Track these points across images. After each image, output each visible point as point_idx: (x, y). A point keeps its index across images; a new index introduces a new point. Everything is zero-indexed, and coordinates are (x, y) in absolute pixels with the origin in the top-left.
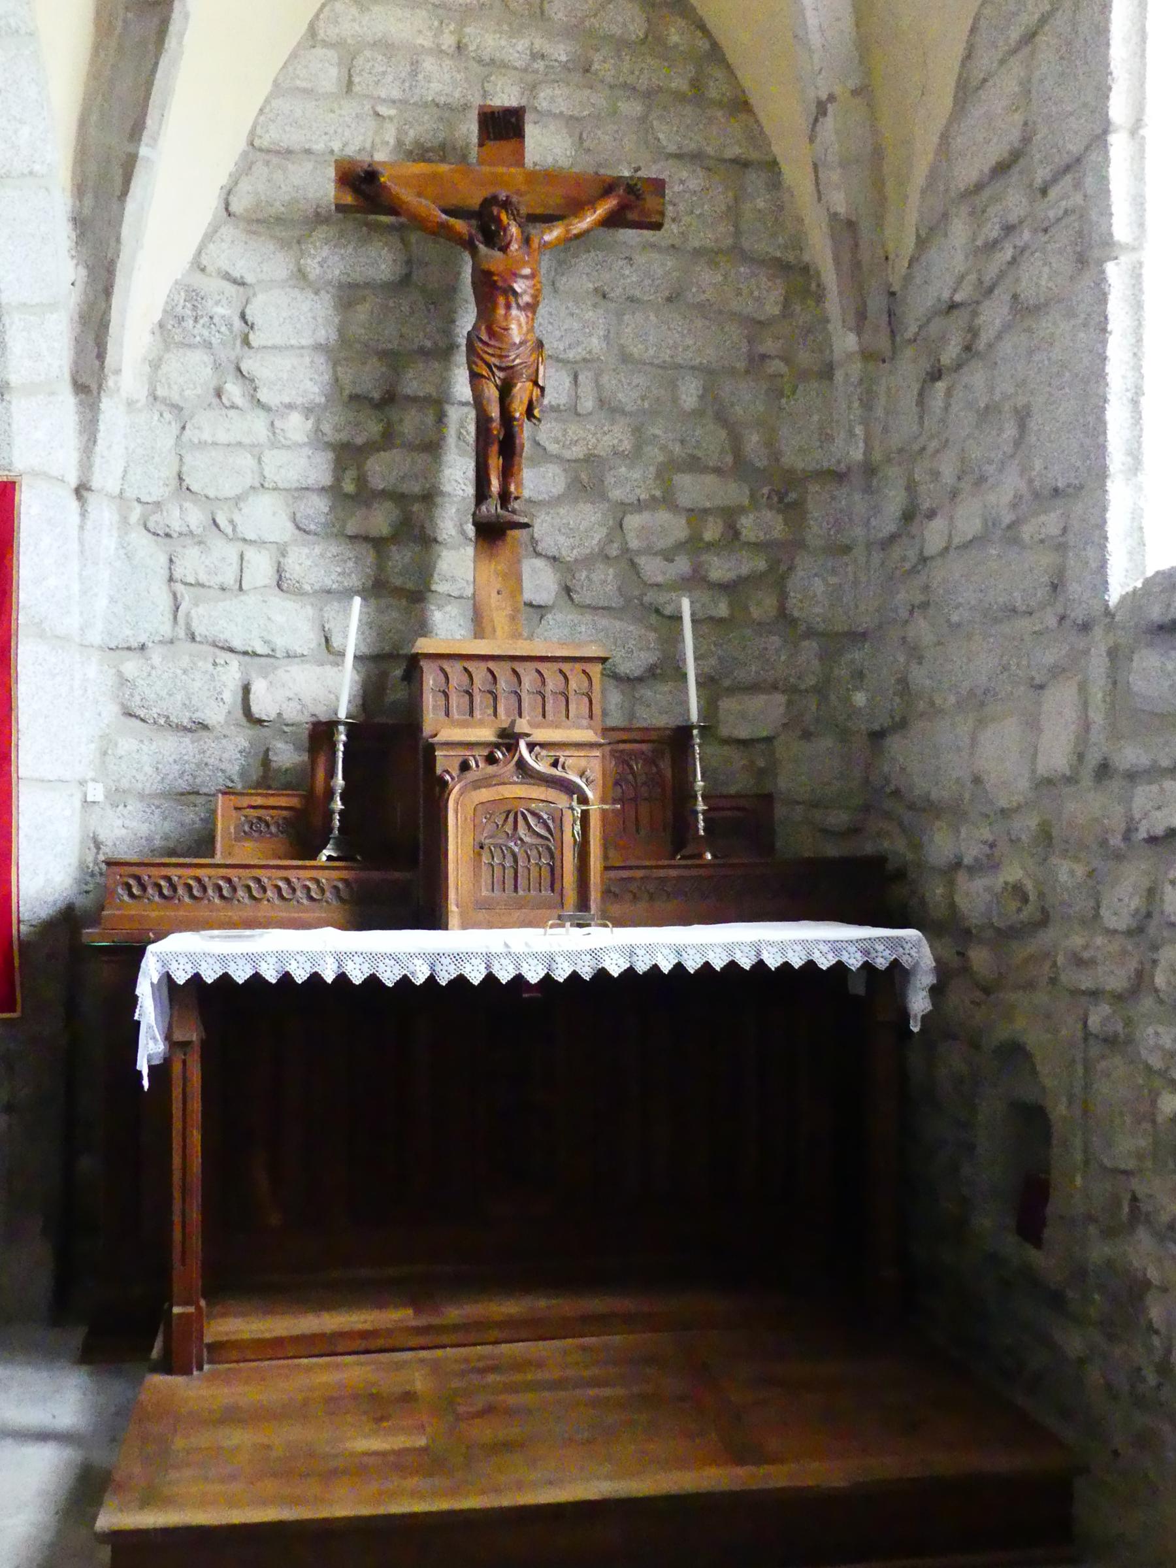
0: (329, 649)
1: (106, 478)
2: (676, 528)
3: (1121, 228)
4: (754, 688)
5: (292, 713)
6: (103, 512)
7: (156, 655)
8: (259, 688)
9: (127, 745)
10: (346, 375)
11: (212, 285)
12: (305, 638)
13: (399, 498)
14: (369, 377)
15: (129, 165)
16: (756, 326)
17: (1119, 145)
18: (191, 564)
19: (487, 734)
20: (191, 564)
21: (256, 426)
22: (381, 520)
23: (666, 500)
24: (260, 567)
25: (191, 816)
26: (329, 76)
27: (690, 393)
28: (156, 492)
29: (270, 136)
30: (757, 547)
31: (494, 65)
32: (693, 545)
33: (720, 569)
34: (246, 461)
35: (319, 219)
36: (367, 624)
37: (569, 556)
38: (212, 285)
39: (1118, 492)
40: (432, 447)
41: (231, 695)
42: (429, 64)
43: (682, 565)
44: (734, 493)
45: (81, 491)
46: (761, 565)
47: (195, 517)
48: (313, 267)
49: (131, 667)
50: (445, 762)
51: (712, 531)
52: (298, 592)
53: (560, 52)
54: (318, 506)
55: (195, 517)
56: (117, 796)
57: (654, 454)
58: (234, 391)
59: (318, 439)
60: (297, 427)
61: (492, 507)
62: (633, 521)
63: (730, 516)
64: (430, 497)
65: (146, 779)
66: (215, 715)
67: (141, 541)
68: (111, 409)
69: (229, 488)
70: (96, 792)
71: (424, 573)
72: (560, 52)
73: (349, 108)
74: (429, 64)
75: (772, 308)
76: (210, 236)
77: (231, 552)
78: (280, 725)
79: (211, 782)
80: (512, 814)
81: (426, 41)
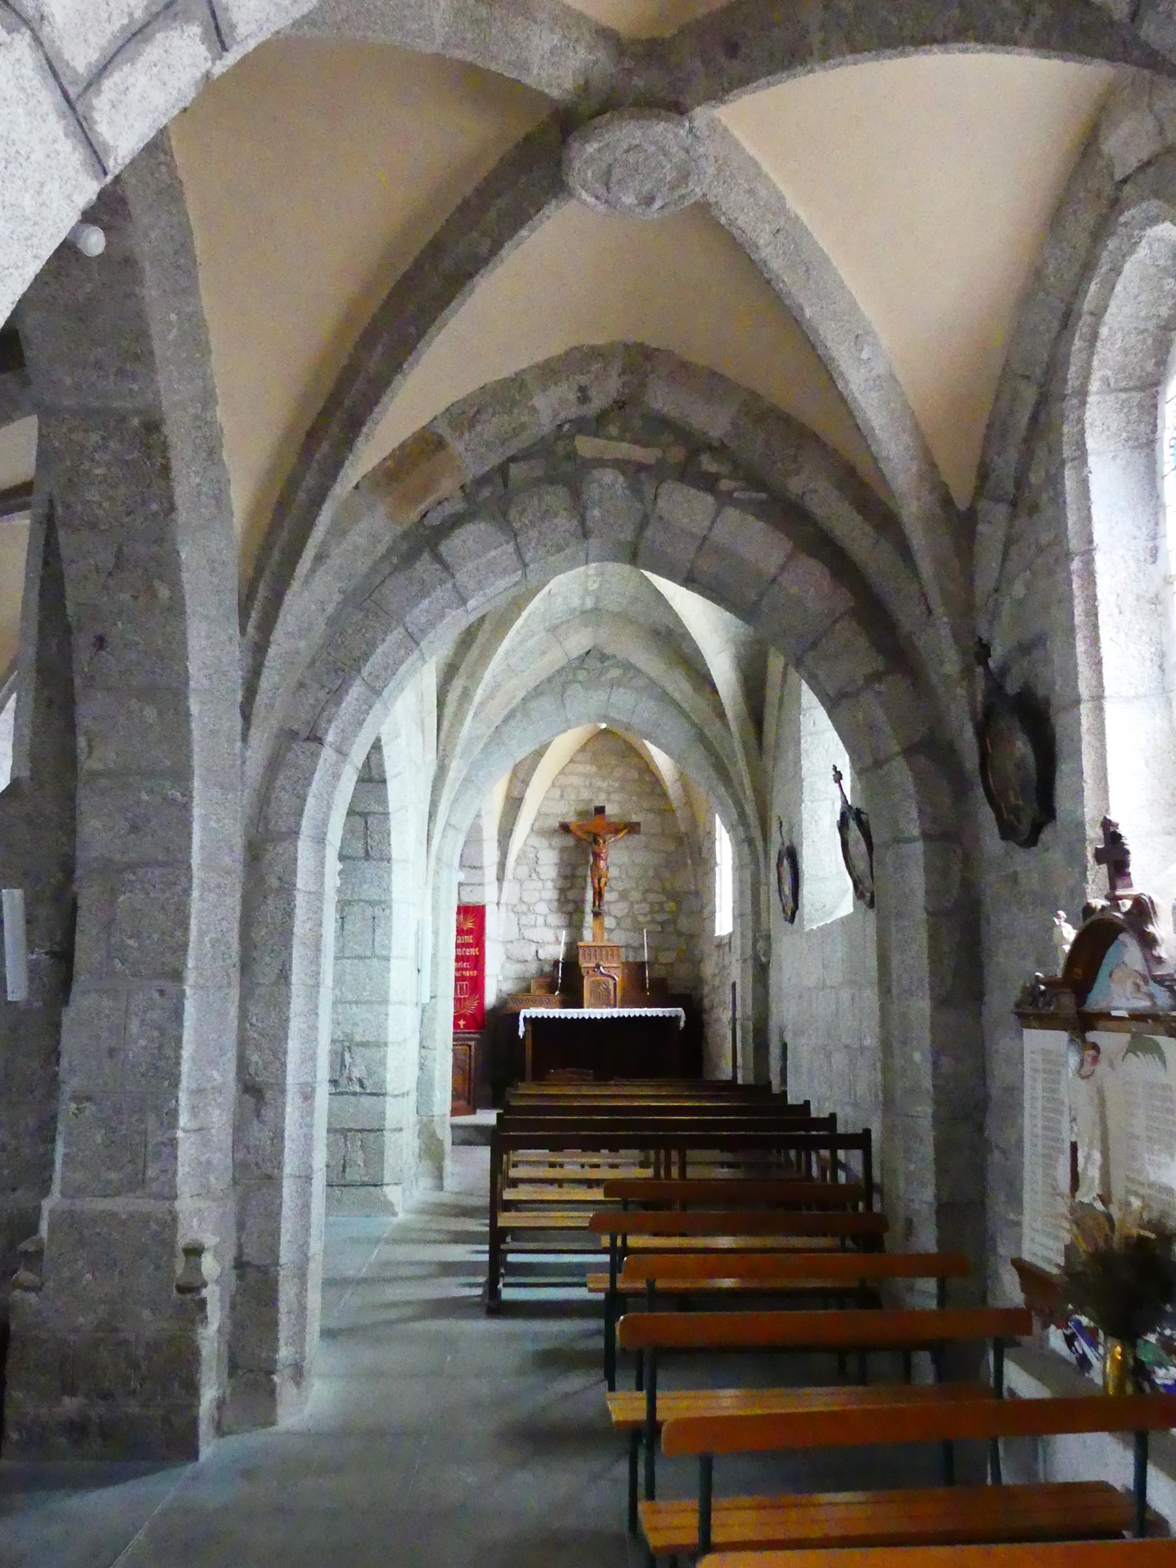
0: (558, 942)
1: (503, 901)
2: (647, 908)
3: (718, 861)
4: (668, 949)
5: (549, 958)
6: (503, 908)
7: (515, 943)
8: (540, 951)
9: (508, 966)
10: (565, 857)
11: (528, 849)
12: (552, 938)
13: (575, 902)
14: (568, 872)
15: (511, 830)
16: (669, 854)
17: (717, 843)
18: (524, 920)
19: (593, 965)
20: (524, 920)
21: (539, 885)
22: (570, 907)
23: (644, 900)
24: (541, 920)
25: (524, 984)
26: (557, 793)
27: (651, 873)
28: (515, 902)
29: (543, 810)
30: (670, 912)
31: (599, 789)
32: (651, 912)
33: (659, 918)
34: (537, 894)
35: (555, 831)
36: (568, 935)
37: (619, 916)
38: (528, 849)
39: (717, 915)
40: (584, 888)
41: (533, 953)
42: (582, 790)
43: (649, 918)
44: (663, 898)
45: (498, 904)
46: (670, 917)
47: (525, 908)
48: (554, 843)
49: (509, 946)
50: (584, 972)
51: (657, 908)
52: (550, 926)
53: (617, 785)
54: (556, 904)
55: (525, 908)
56: (506, 979)
57: (641, 888)
58: (534, 875)
59: (555, 887)
60: (550, 885)
61: (596, 909)
62: (636, 906)
63: (661, 904)
64: (583, 901)
65: (513, 974)
66: (530, 958)
67: (511, 914)
68: (506, 885)
69: (533, 900)
70: (501, 978)
71: (582, 921)
72: (617, 785)
73: (562, 802)
74: (582, 790)
75: (673, 848)
76: (529, 836)
77: (533, 917)
78: (546, 960)
79: (527, 975)
80: (599, 983)
81: (604, 697)
